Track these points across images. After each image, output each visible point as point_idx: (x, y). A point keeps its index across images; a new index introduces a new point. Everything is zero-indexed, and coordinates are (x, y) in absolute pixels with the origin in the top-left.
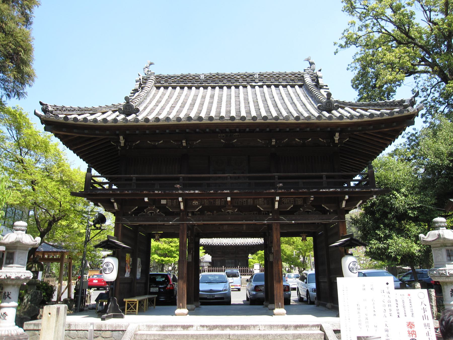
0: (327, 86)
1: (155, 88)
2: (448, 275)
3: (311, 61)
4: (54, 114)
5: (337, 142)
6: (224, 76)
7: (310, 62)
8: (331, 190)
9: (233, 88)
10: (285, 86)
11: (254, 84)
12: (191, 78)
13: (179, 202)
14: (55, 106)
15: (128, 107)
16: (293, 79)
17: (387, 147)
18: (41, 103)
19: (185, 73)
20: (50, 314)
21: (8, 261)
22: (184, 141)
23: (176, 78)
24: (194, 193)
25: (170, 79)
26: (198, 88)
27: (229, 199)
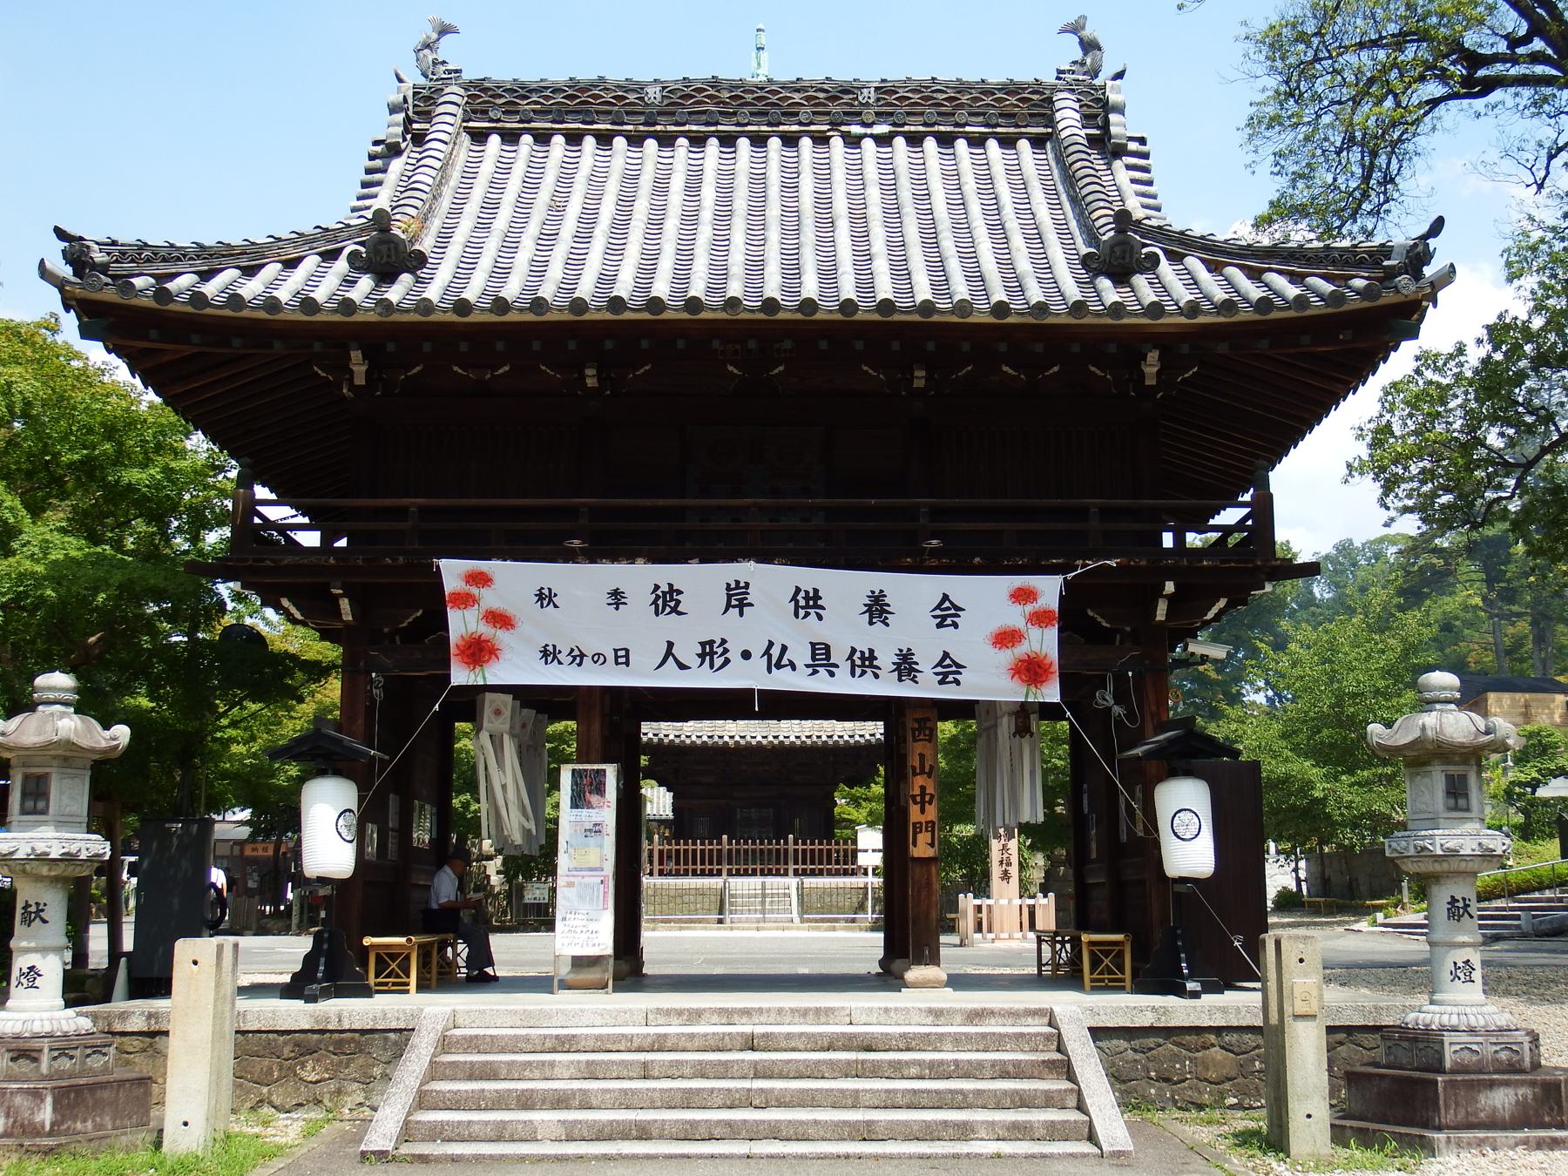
0: (1142, 141)
1: (465, 139)
2: (1439, 852)
3: (1087, 33)
4: (113, 277)
7: (1082, 42)
9: (775, 143)
10: (977, 142)
11: (856, 129)
12: (608, 97)
14: (114, 243)
15: (384, 248)
18: (60, 234)
19: (586, 74)
20: (195, 963)
22: (590, 372)
23: (547, 98)
25: (525, 97)
26: (636, 140)
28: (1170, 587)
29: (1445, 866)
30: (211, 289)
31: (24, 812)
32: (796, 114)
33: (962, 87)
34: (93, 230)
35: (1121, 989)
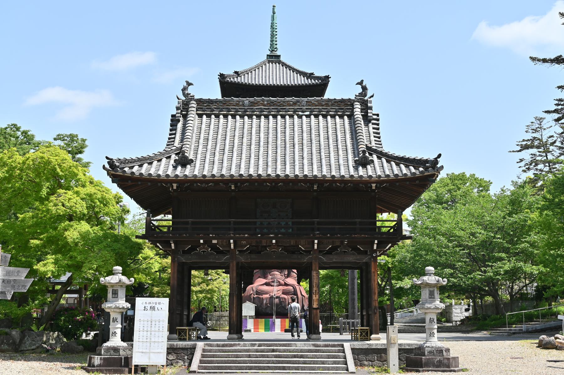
0: (378, 115)
14: (120, 160)
18: (107, 158)
27: (274, 241)
28: (376, 242)
34: (114, 157)
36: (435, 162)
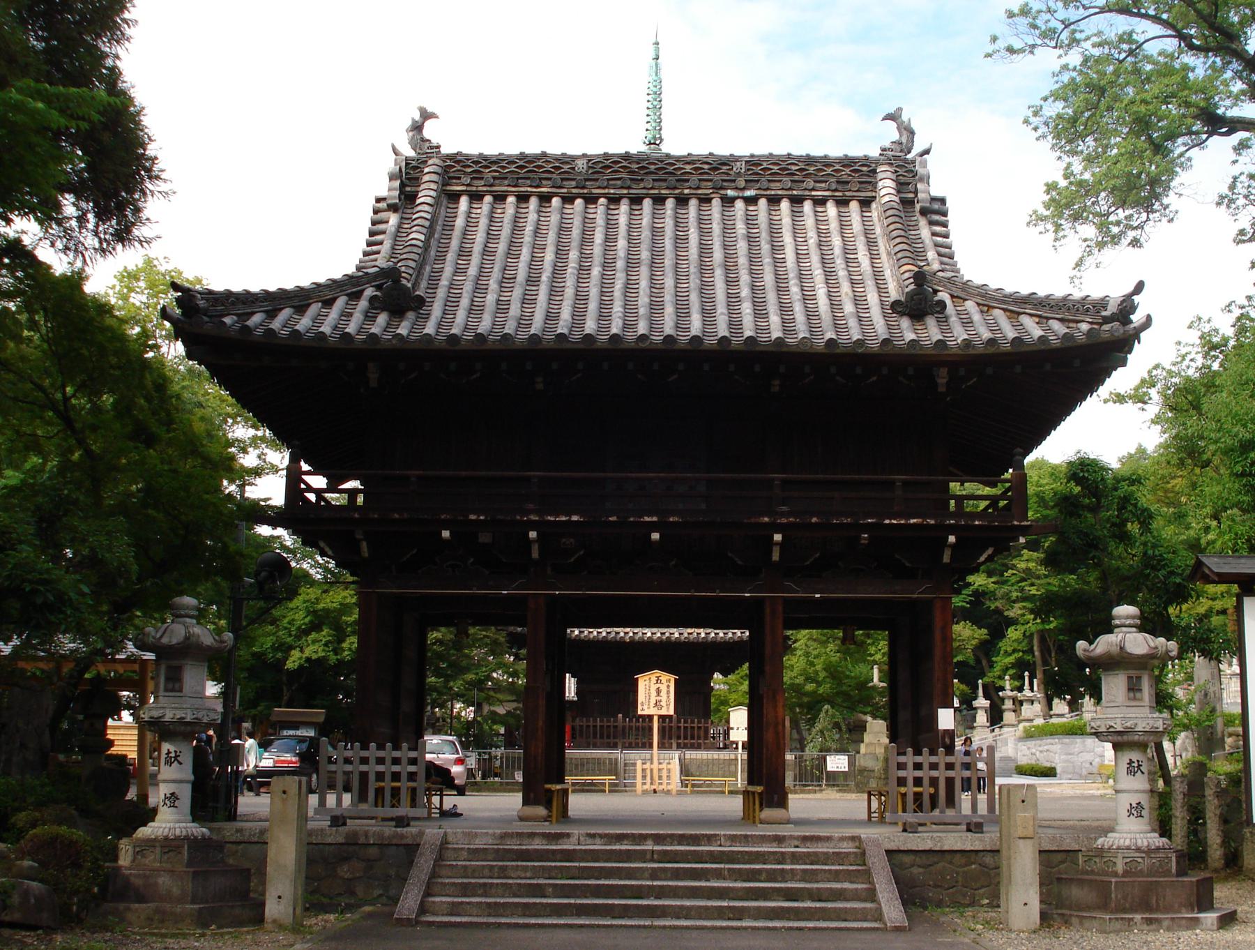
5: (942, 389)
6: (644, 164)
8: (912, 521)
11: (730, 193)
12: (549, 167)
13: (530, 542)
16: (845, 178)
17: (1130, 352)
19: (533, 149)
20: (284, 792)
21: (170, 686)
23: (504, 168)
24: (570, 521)
26: (568, 200)
28: (952, 539)
29: (1125, 738)
30: (276, 324)
31: (166, 690)
32: (687, 181)
33: (810, 160)
35: (850, 791)
36: (1127, 307)
